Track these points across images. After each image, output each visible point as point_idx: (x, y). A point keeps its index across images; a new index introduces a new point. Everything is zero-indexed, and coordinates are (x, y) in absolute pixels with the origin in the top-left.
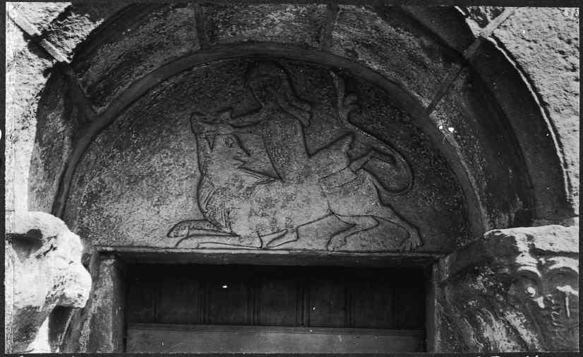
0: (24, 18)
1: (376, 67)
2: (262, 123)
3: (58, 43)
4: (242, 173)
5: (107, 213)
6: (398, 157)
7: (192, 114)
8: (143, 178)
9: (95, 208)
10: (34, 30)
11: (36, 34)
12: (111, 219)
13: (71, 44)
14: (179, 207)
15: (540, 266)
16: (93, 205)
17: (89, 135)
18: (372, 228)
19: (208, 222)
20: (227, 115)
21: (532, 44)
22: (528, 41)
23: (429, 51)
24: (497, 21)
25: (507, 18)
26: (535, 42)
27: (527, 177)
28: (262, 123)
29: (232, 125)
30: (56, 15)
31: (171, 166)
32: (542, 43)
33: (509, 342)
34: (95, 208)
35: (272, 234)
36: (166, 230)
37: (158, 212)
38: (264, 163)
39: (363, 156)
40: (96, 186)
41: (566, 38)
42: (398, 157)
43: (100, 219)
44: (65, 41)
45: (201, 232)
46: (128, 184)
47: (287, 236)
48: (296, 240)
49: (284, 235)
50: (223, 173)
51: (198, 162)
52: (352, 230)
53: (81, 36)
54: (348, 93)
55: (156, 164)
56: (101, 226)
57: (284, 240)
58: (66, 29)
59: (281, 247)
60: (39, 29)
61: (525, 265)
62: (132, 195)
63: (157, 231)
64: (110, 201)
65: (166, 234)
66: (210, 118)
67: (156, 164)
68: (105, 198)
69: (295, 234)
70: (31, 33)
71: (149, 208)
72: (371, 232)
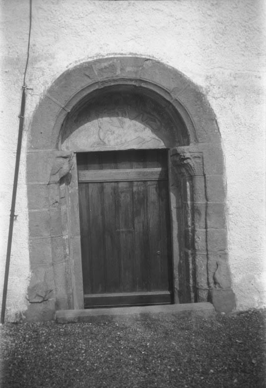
6: (156, 120)
15: (191, 156)
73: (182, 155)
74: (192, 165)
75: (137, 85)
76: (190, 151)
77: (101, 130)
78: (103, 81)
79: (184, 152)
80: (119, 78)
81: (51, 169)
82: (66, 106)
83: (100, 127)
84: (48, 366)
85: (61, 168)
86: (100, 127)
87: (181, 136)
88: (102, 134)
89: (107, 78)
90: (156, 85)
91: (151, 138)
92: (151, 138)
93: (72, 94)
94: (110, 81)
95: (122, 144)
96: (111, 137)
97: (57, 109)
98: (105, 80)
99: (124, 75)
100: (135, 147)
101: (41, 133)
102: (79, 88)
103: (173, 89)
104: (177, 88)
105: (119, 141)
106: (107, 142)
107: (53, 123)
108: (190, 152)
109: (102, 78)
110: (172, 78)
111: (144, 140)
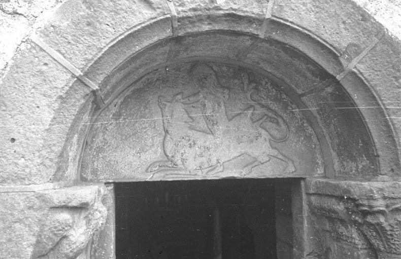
0: (72, 65)
1: (269, 71)
2: (201, 101)
3: (93, 78)
4: (190, 132)
5: (109, 159)
6: (280, 120)
7: (159, 97)
8: (130, 137)
9: (101, 156)
10: (79, 73)
11: (80, 75)
12: (111, 162)
13: (101, 78)
14: (152, 155)
15: (387, 206)
16: (100, 154)
17: (99, 113)
18: (267, 162)
19: (168, 161)
20: (179, 97)
21: (378, 73)
22: (376, 71)
23: (312, 72)
24: (358, 59)
25: (364, 57)
26: (380, 71)
27: (374, 149)
28: (201, 101)
29: (183, 103)
30: (93, 62)
31: (147, 129)
32: (384, 72)
33: (360, 241)
34: (101, 156)
35: (208, 168)
36: (145, 167)
37: (140, 157)
38: (202, 125)
39: (260, 119)
40: (102, 142)
41: (397, 69)
42: (280, 120)
43: (105, 163)
44: (98, 77)
45: (166, 168)
46: (121, 140)
47: (217, 168)
48: (222, 172)
49: (214, 168)
50: (178, 129)
51: (163, 126)
52: (256, 163)
53: (107, 72)
54: (250, 82)
55: (138, 128)
56: (105, 167)
57: (216, 171)
58: (98, 69)
59: (214, 175)
60: (82, 71)
61: (380, 207)
62: (124, 147)
63: (140, 169)
64: (110, 151)
65: (144, 170)
66: (169, 98)
67: (138, 128)
68: (108, 149)
69: (222, 167)
70: (77, 75)
71: (134, 154)
72: (266, 164)
73: (366, 202)
74: (388, 228)
75: (262, 36)
76: (386, 195)
77: (168, 137)
78: (183, 18)
79: (371, 198)
80: (222, 12)
81: (33, 240)
82: (86, 74)
83: (167, 132)
84: (43, 237)
85: (65, 237)
86: (167, 132)
87: (334, 154)
88: (169, 146)
89: (194, 10)
90: (308, 37)
91: (268, 155)
92: (268, 155)
93: (105, 43)
94: (200, 19)
95: (213, 168)
96: (190, 153)
97: (63, 81)
98: (190, 14)
99: (235, 7)
100: (236, 173)
101: (13, 140)
102: (122, 31)
103: (346, 48)
104: (355, 45)
105: (204, 159)
106: (179, 162)
107: (47, 116)
108: (385, 198)
109: (180, 9)
110: (344, 23)
111: (255, 160)
